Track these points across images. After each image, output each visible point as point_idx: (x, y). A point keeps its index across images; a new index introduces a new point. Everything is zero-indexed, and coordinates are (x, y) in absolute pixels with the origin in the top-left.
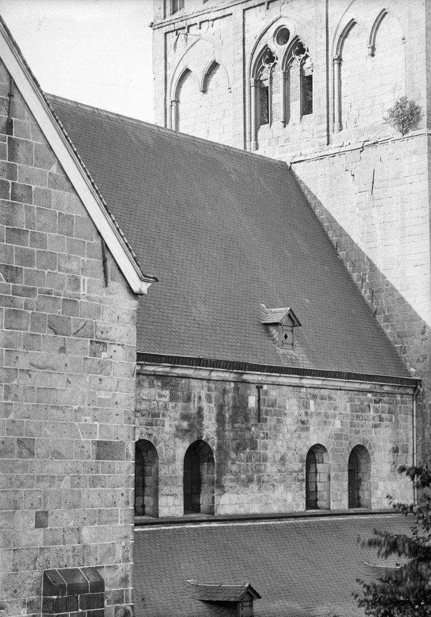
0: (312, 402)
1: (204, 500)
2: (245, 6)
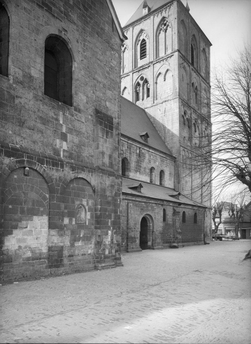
0: (152, 156)
1: (127, 173)
2: (133, 72)
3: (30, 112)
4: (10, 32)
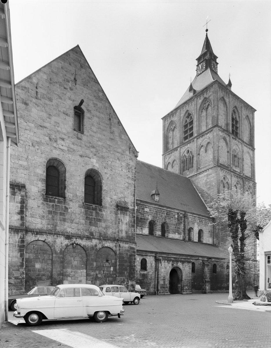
1: (166, 235)
3: (77, 215)
4: (66, 175)
